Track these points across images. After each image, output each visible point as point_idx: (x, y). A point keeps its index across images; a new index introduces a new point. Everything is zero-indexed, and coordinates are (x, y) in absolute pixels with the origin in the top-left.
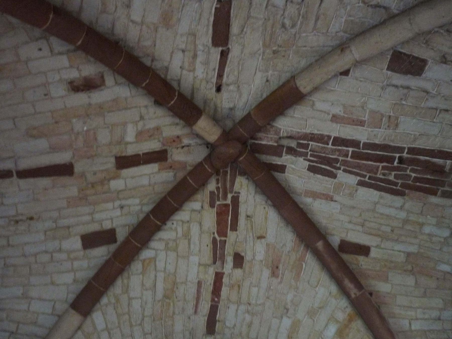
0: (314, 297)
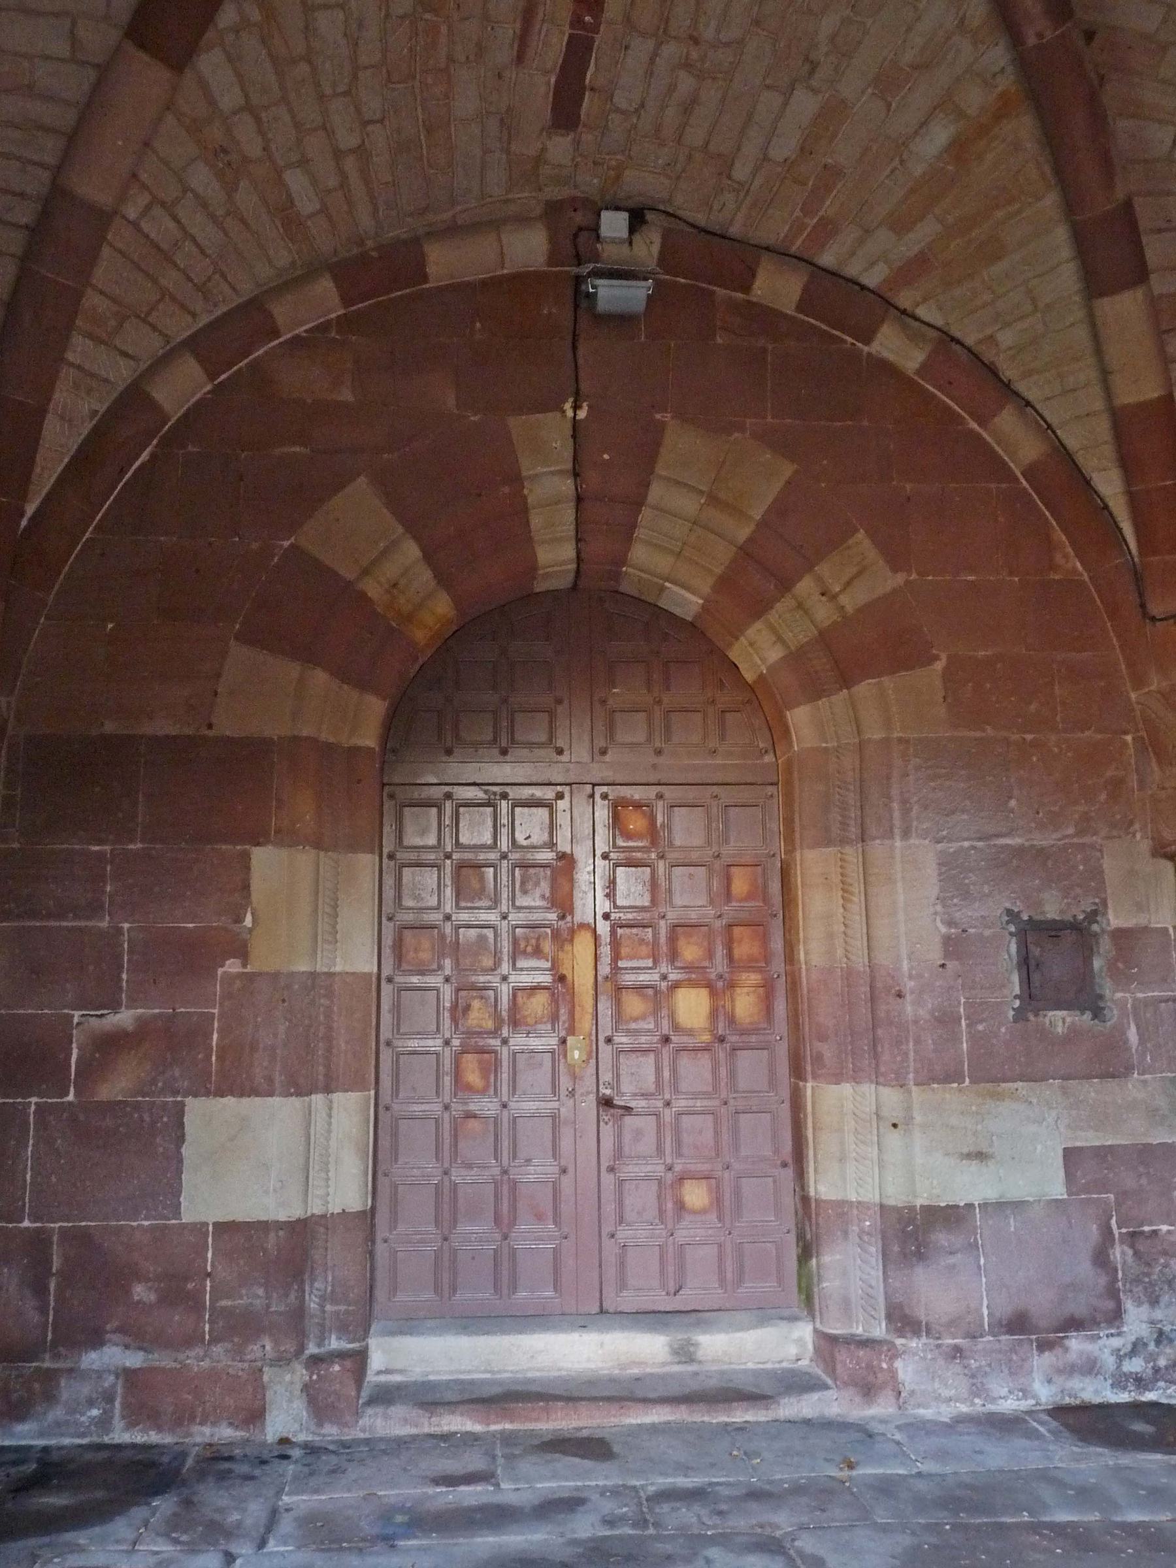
0: (909, 29)
